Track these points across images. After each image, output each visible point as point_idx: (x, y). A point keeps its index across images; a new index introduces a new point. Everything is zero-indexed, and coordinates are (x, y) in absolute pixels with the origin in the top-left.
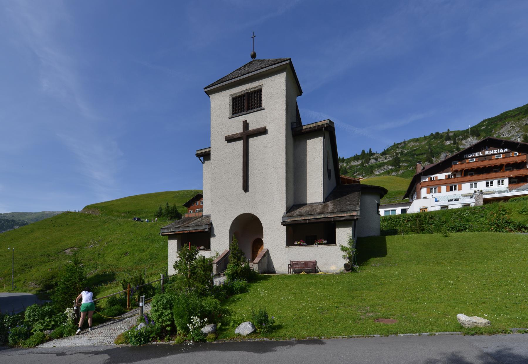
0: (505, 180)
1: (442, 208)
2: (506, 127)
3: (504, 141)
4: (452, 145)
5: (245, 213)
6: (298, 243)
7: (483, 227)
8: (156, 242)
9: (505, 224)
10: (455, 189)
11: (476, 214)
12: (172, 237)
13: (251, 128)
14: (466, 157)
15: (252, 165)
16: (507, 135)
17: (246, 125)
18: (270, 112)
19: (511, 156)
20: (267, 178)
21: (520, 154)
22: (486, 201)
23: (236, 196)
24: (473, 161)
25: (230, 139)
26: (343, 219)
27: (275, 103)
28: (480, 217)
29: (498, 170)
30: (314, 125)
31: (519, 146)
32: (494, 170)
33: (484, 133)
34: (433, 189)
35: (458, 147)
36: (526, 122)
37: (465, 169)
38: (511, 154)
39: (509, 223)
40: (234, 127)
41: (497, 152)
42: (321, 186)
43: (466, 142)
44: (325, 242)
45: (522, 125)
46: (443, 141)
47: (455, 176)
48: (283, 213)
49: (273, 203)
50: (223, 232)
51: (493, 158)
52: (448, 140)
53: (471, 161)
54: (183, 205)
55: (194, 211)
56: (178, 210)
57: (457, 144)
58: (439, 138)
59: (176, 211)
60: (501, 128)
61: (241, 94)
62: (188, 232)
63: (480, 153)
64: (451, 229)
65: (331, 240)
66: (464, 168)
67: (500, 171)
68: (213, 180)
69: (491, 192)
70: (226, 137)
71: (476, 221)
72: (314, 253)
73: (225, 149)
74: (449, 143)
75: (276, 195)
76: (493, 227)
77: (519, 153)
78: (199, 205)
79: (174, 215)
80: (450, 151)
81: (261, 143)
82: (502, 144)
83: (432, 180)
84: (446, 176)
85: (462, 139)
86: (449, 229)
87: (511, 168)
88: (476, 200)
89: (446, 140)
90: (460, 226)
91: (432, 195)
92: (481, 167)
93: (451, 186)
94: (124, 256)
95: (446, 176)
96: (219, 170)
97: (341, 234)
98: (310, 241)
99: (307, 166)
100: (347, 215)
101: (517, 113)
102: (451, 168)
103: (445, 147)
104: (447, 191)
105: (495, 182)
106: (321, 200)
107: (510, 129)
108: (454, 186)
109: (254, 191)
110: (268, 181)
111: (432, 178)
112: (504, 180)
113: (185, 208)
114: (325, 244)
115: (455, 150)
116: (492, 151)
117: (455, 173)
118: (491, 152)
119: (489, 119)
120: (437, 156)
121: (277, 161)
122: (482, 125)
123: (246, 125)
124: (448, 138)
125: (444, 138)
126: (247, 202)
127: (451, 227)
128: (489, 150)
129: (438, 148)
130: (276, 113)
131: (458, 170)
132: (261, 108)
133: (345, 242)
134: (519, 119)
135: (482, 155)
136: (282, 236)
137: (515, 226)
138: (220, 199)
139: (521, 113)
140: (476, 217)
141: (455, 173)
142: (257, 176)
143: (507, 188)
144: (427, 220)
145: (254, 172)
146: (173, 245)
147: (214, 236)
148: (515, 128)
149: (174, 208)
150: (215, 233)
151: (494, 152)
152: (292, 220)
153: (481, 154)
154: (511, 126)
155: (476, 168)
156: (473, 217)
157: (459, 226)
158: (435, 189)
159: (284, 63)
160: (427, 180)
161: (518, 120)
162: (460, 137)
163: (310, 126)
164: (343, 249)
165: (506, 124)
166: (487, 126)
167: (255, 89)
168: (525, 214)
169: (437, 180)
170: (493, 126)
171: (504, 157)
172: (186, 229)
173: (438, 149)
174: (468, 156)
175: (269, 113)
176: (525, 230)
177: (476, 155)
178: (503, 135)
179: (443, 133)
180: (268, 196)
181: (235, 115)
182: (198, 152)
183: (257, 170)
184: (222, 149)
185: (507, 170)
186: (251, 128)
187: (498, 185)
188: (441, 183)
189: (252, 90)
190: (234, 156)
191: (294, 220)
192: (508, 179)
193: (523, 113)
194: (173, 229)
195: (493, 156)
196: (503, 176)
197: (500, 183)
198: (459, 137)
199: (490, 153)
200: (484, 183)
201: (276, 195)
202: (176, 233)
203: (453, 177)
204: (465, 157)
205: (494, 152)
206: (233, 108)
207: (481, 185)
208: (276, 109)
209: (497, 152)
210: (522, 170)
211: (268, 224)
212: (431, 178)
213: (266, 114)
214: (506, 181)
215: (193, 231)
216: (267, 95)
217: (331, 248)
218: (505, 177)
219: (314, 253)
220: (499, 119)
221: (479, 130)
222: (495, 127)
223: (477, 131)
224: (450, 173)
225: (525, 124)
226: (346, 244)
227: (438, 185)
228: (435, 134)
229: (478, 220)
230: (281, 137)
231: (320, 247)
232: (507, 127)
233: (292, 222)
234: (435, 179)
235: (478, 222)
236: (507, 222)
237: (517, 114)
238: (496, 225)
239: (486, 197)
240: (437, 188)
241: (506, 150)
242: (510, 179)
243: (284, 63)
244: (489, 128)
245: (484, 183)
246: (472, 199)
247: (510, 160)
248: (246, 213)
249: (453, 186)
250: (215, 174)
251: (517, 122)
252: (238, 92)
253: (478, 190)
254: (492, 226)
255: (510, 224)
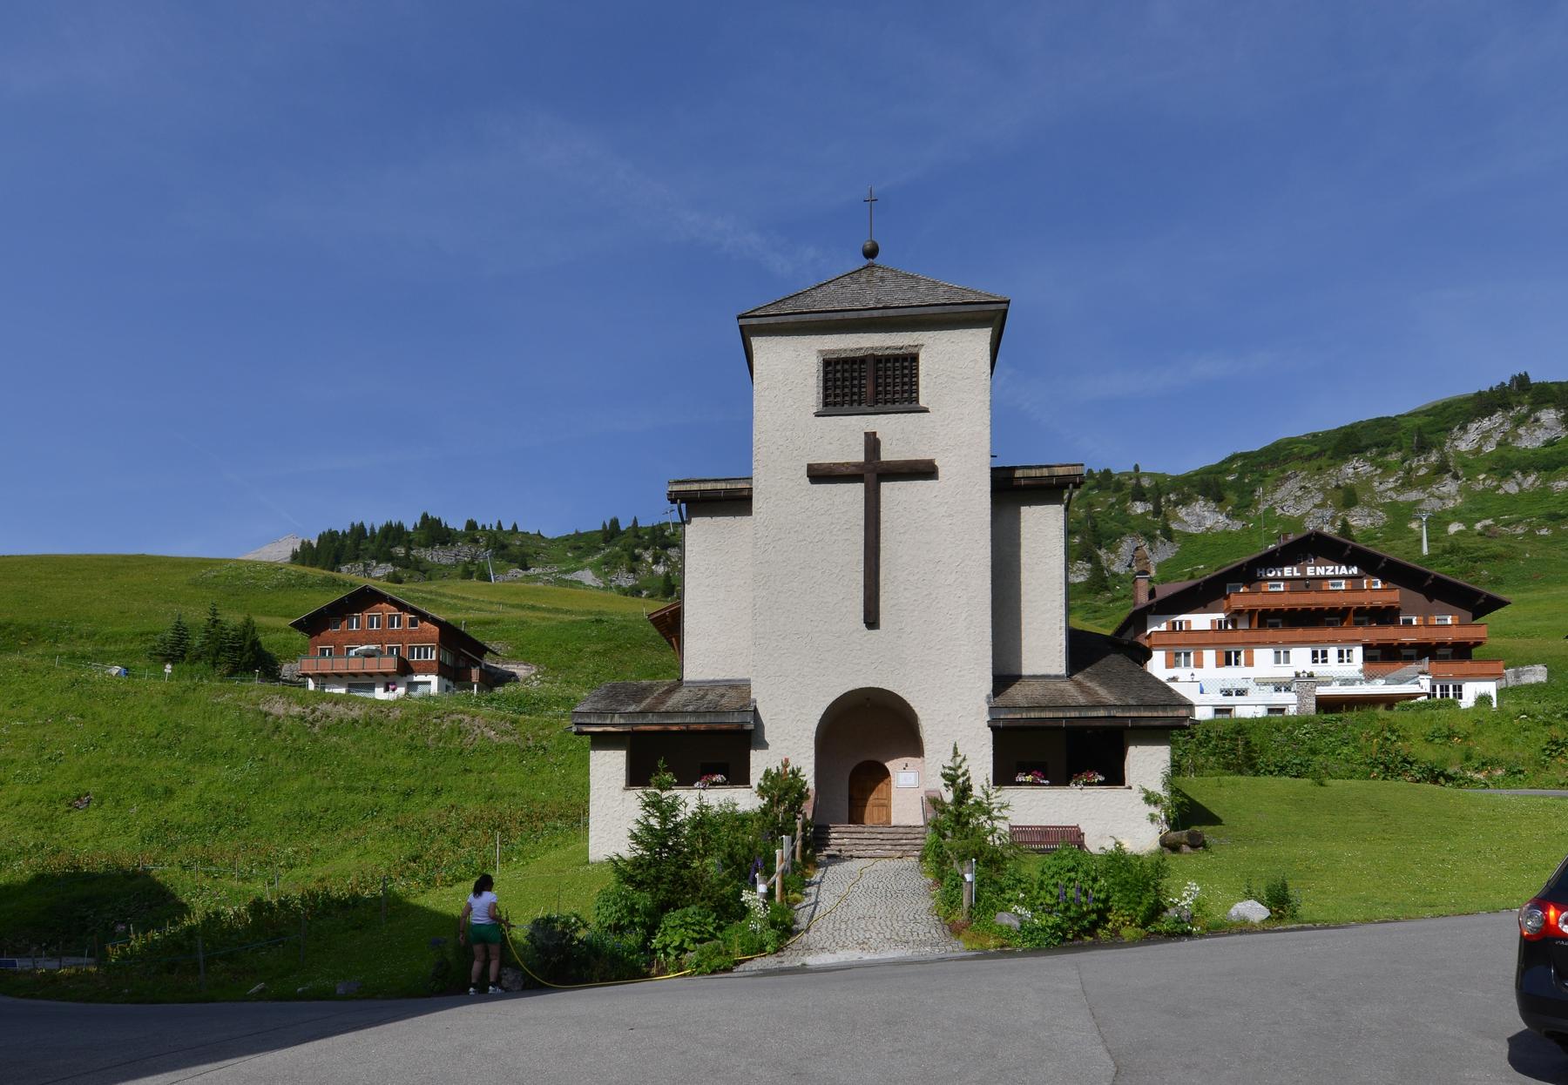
0: (1354, 650)
1: (1270, 711)
2: (1289, 485)
3: (1385, 560)
4: (1149, 518)
5: (868, 686)
6: (1029, 778)
7: (1354, 771)
8: (219, 761)
9: (1401, 764)
10: (1237, 663)
11: (1331, 736)
12: (604, 741)
13: (886, 455)
14: (1261, 574)
15: (889, 556)
16: (1292, 511)
17: (872, 443)
18: (946, 423)
19: (1365, 587)
20: (936, 598)
21: (1386, 586)
22: (1328, 705)
23: (839, 637)
24: (1278, 589)
25: (820, 475)
26: (1157, 723)
27: (959, 401)
28: (1340, 743)
29: (1337, 621)
30: (1045, 472)
31: (1348, 552)
32: (1327, 619)
33: (1235, 493)
34: (1183, 654)
35: (1168, 525)
36: (1338, 481)
37: (1260, 609)
38: (1365, 581)
39: (1411, 764)
40: (832, 441)
41: (1333, 573)
42: (1058, 632)
43: (1187, 514)
44: (1101, 778)
45: (1329, 488)
46: (1125, 501)
47: (1234, 623)
48: (985, 695)
49: (955, 667)
50: (794, 737)
51: (1324, 589)
52: (1141, 501)
53: (1272, 589)
54: (294, 625)
55: (340, 652)
56: (261, 638)
57: (1165, 515)
58: (1112, 488)
59: (255, 644)
60: (1276, 488)
61: (852, 355)
62: (684, 728)
63: (1295, 569)
64: (1279, 771)
65: (1115, 777)
66: (1258, 606)
67: (1342, 623)
68: (761, 584)
69: (1325, 680)
70: (810, 467)
71: (1333, 754)
72: (1072, 807)
73: (802, 500)
74: (1143, 511)
75: (964, 645)
76: (1376, 770)
77: (1383, 583)
78: (363, 629)
79: (245, 659)
80: (1145, 535)
81: (916, 500)
82: (1380, 567)
83: (1178, 629)
84: (1213, 622)
85: (1176, 504)
86: (1274, 771)
87: (1366, 618)
88: (1300, 698)
89: (1134, 500)
90: (1301, 764)
91: (1193, 675)
92: (1313, 608)
93: (1226, 652)
94: (69, 811)
95: (1213, 622)
96: (782, 555)
97: (1143, 762)
98: (1061, 777)
99: (1022, 575)
100: (1165, 715)
101: (1316, 449)
102: (1225, 602)
103: (1132, 521)
104: (1218, 666)
105: (1333, 652)
106: (1061, 669)
107: (1299, 493)
108: (1235, 652)
109: (898, 628)
110: (939, 606)
111: (1178, 623)
112: (1352, 651)
113: (299, 638)
114: (1100, 783)
115: (1158, 532)
116: (1323, 568)
117: (1235, 616)
118: (1321, 571)
119: (1244, 456)
120: (1111, 544)
121: (967, 555)
122: (1228, 469)
123: (872, 443)
124: (1139, 494)
125: (1125, 491)
126: (876, 657)
127: (1277, 766)
128: (1315, 565)
129: (1112, 519)
130: (962, 430)
131: (1243, 610)
132: (913, 405)
133: (1152, 780)
134: (1319, 469)
135: (1299, 574)
136: (980, 757)
137: (1423, 772)
138: (783, 639)
139: (1325, 451)
140: (1331, 742)
141: (1235, 616)
142: (905, 589)
143: (1360, 671)
144: (1213, 743)
145: (895, 577)
146: (608, 767)
147: (763, 745)
148: (1310, 492)
149: (245, 634)
150: (767, 739)
151: (1326, 570)
152: (1018, 716)
153: (1296, 574)
154: (1302, 484)
155: (1286, 608)
156: (1323, 744)
157: (1296, 764)
158: (1187, 655)
159: (993, 307)
160: (1164, 627)
161: (1318, 469)
162: (1171, 495)
163: (1033, 473)
164: (1150, 799)
165: (1288, 478)
166: (1241, 476)
167: (897, 352)
168: (1441, 744)
169: (1189, 631)
170: (1255, 477)
171: (1349, 587)
172: (672, 719)
173: (1113, 525)
174: (1266, 574)
175: (942, 426)
176: (1447, 782)
177: (1286, 575)
178: (1282, 508)
179: (1121, 474)
180: (939, 647)
181: (831, 409)
182: (676, 488)
183: (906, 572)
184: (793, 497)
185: (1358, 624)
186: (886, 455)
187: (1339, 662)
188: (1199, 641)
189: (887, 352)
190: (832, 523)
191: (1024, 716)
192: (1361, 648)
193: (1329, 453)
194: (620, 717)
195: (1324, 583)
196: (1351, 638)
197: (1343, 657)
198: (1168, 494)
199: (1318, 574)
200: (1307, 652)
201: (964, 645)
202: (635, 728)
203: (1230, 627)
204: (1258, 575)
205: (1326, 570)
206: (826, 388)
207: (1301, 658)
208: (962, 419)
209: (1333, 573)
210: (1392, 628)
211: (940, 722)
212: (1174, 623)
213: (932, 425)
214: (1358, 652)
215: (703, 728)
216: (935, 376)
217: (1118, 796)
218: (1355, 642)
219: (1072, 807)
220: (1271, 460)
221: (1220, 482)
222: (1261, 481)
223: (1217, 484)
224: (1222, 616)
225: (1336, 486)
226: (1157, 787)
227: (1196, 647)
228: (1101, 474)
229: (1339, 751)
230: (977, 495)
231: (1089, 790)
232: (1292, 486)
233: (1021, 723)
234: (1184, 629)
235: (1339, 757)
236: (1405, 760)
237: (1315, 453)
238: (1382, 767)
239: (1322, 691)
240: (1192, 654)
241: (1355, 570)
242: (1366, 647)
243: (993, 307)
244: (1247, 481)
245: (1307, 652)
246: (1289, 694)
247: (1365, 600)
248: (870, 688)
249: (1233, 654)
250: (767, 565)
251: (1317, 477)
252: (845, 348)
253: (1304, 672)
254: (1374, 767)
255: (1411, 766)
